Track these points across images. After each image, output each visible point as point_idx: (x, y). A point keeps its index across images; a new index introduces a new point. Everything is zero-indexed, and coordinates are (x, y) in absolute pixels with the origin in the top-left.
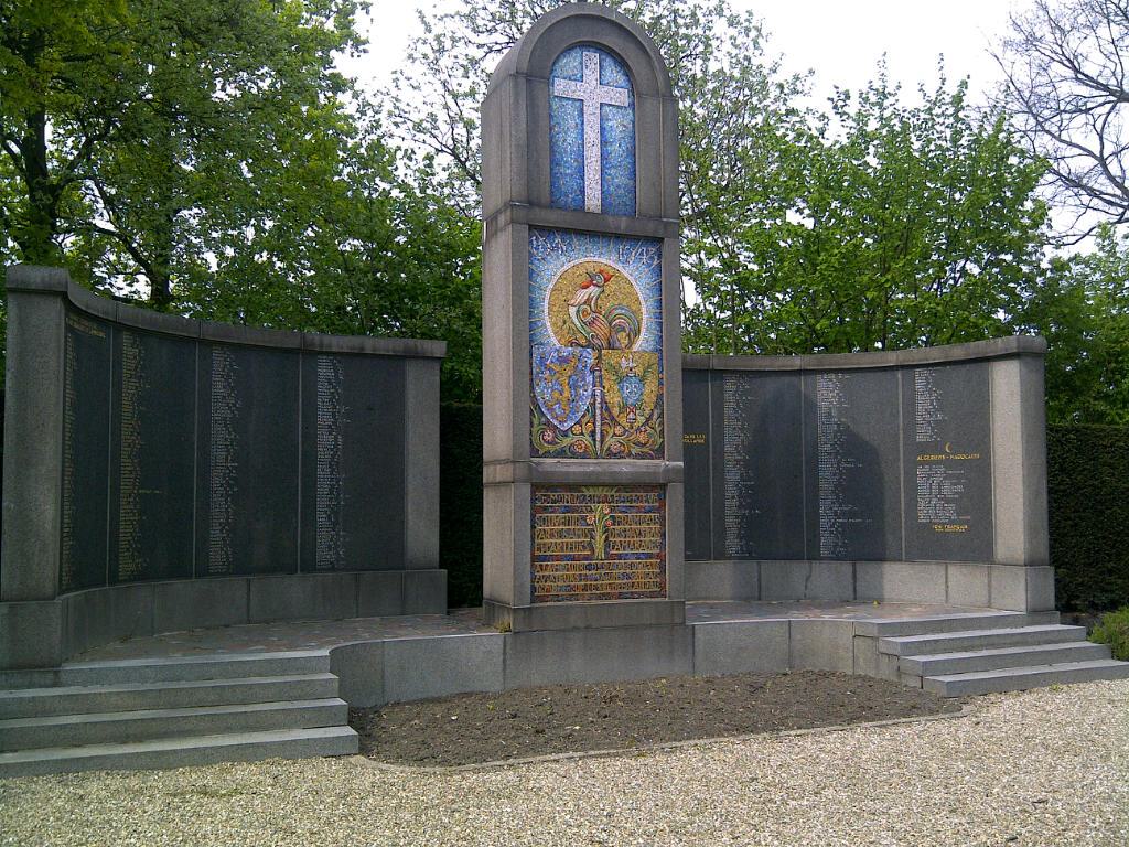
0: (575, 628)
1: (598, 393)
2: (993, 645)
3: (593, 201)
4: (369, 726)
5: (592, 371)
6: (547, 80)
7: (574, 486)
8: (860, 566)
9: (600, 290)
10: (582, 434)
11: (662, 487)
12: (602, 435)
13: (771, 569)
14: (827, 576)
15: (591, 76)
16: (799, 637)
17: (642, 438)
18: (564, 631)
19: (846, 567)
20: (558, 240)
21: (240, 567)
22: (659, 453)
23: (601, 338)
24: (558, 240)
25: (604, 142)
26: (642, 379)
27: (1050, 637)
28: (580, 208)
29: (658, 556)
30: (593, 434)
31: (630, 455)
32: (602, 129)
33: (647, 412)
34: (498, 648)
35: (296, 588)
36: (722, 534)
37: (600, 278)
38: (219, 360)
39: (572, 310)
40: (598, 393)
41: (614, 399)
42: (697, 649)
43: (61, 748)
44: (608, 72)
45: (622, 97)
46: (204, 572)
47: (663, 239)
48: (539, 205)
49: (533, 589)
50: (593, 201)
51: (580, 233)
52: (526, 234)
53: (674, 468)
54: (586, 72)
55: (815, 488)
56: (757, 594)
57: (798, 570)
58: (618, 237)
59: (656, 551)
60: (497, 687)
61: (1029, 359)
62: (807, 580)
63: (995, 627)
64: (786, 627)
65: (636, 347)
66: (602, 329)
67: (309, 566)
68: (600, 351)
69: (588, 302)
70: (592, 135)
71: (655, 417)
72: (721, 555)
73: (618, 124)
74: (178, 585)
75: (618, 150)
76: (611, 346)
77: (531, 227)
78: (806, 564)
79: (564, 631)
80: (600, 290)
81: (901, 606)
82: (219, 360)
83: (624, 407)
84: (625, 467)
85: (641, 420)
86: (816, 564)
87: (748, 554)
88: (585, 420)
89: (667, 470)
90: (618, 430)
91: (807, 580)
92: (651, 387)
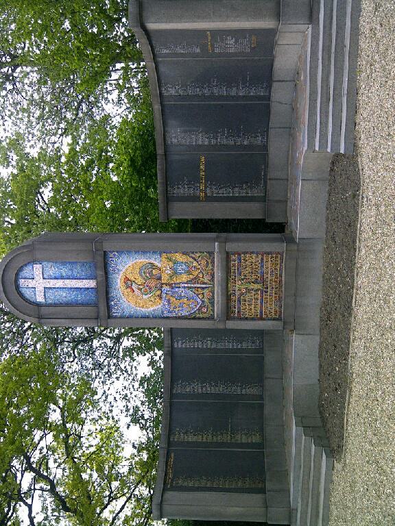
0: (295, 301)
1: (183, 285)
2: (327, 86)
3: (92, 284)
4: (327, 433)
5: (173, 288)
6: (39, 305)
7: (228, 297)
8: (276, 77)
9: (134, 283)
10: (203, 294)
11: (228, 255)
12: (204, 283)
13: (274, 121)
14: (279, 94)
15: (31, 283)
16: (311, 174)
17: (203, 262)
18: (296, 305)
19: (275, 85)
20: (112, 303)
21: (260, 381)
22: (211, 254)
23: (153, 282)
24: (112, 303)
25: (62, 278)
26: (175, 263)
27: (328, 22)
28: (95, 289)
29: (263, 255)
30: (203, 288)
31: (213, 270)
32: (56, 278)
33: (191, 260)
34: (301, 337)
35: (270, 358)
36: (250, 147)
37: (128, 282)
38: (178, 390)
39: (145, 297)
40: (183, 285)
41: (184, 278)
42: (311, 237)
43: (320, 513)
44: (27, 275)
45: (37, 268)
46: (261, 398)
47: (104, 252)
48: (98, 312)
49: (274, 319)
50: (92, 284)
51: (107, 293)
52: (113, 320)
53: (219, 249)
54: (30, 286)
55: (228, 98)
56: (288, 129)
57: (275, 108)
58: (106, 273)
59: (260, 256)
60: (318, 338)
61: (144, 14)
62: (281, 103)
63: (317, 56)
64: (305, 182)
65: (159, 265)
66: (153, 283)
67: (260, 350)
68: (163, 284)
69: (140, 290)
70: (59, 283)
71: (193, 256)
72: (265, 147)
73: (52, 270)
74: (266, 411)
75: (64, 271)
76: (160, 278)
77: (109, 317)
78: (273, 105)
79: (296, 305)
80: (134, 283)
81: (301, 58)
82: (178, 390)
83: (189, 273)
84: (218, 274)
85: (195, 264)
86: (273, 99)
87: (266, 133)
88: (197, 292)
89: (220, 252)
90: (201, 275)
91: (281, 103)
92: (179, 257)
